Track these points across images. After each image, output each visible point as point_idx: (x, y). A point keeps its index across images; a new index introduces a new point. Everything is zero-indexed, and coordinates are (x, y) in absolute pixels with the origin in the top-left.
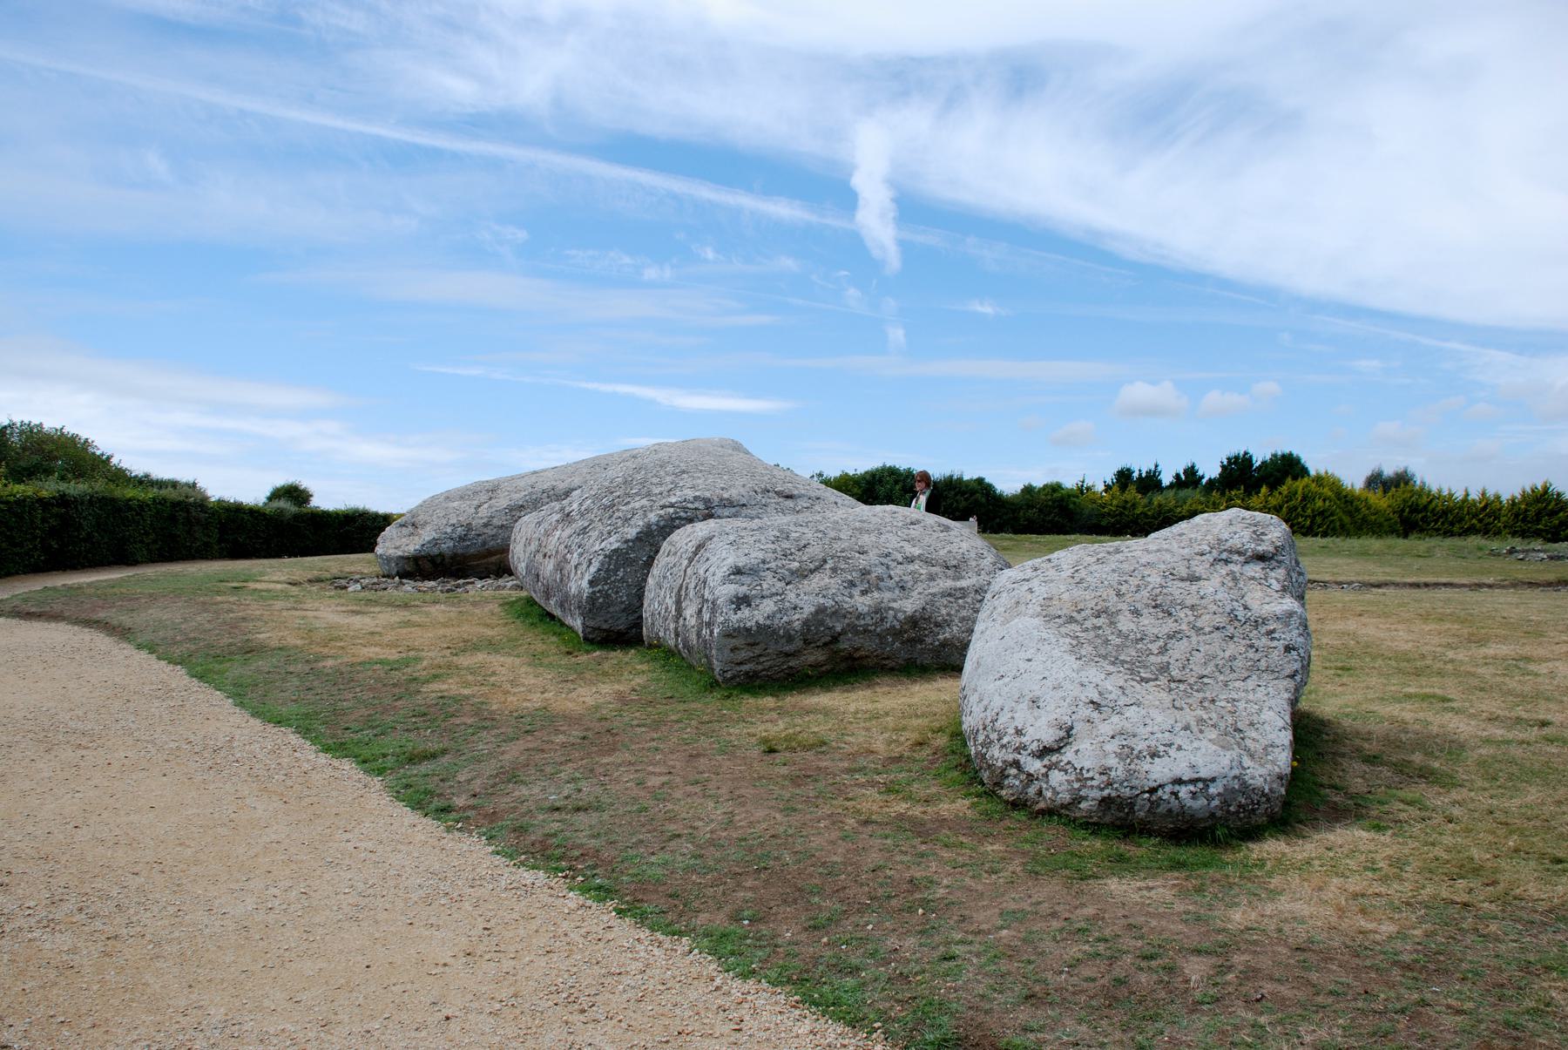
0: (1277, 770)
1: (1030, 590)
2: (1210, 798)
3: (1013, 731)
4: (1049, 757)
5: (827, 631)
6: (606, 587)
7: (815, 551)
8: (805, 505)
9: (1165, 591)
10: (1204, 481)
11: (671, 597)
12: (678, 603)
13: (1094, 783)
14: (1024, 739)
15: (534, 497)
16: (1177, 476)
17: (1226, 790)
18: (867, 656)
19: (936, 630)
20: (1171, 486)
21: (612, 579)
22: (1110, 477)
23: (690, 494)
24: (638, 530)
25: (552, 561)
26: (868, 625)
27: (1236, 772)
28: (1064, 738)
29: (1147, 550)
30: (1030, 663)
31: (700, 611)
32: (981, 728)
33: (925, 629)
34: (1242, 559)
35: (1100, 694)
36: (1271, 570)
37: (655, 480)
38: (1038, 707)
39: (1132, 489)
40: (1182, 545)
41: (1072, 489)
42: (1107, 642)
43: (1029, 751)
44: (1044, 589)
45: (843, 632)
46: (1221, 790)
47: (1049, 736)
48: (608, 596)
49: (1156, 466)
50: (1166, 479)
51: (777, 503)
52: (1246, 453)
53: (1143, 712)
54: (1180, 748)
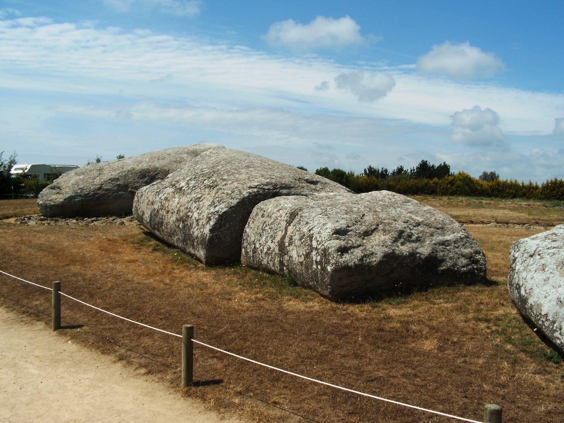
6: (219, 233)
7: (369, 218)
8: (321, 187)
15: (124, 174)
21: (223, 228)
24: (238, 201)
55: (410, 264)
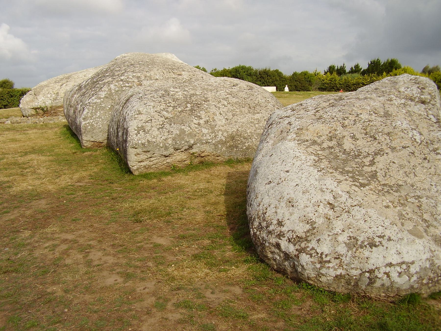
1: (290, 123)
5: (186, 143)
6: (91, 121)
9: (371, 124)
10: (362, 70)
13: (331, 265)
14: (283, 229)
16: (352, 68)
17: (421, 269)
18: (208, 155)
19: (244, 141)
20: (349, 73)
21: (94, 117)
22: (326, 69)
26: (208, 139)
29: (358, 98)
30: (288, 174)
33: (238, 140)
34: (413, 103)
35: (335, 198)
38: (293, 206)
39: (335, 74)
40: (379, 95)
41: (312, 74)
42: (336, 157)
44: (298, 123)
45: (195, 144)
46: (418, 269)
48: (92, 125)
49: (344, 65)
50: (348, 70)
52: (378, 60)
53: (363, 211)
54: (389, 239)
55: (211, 140)
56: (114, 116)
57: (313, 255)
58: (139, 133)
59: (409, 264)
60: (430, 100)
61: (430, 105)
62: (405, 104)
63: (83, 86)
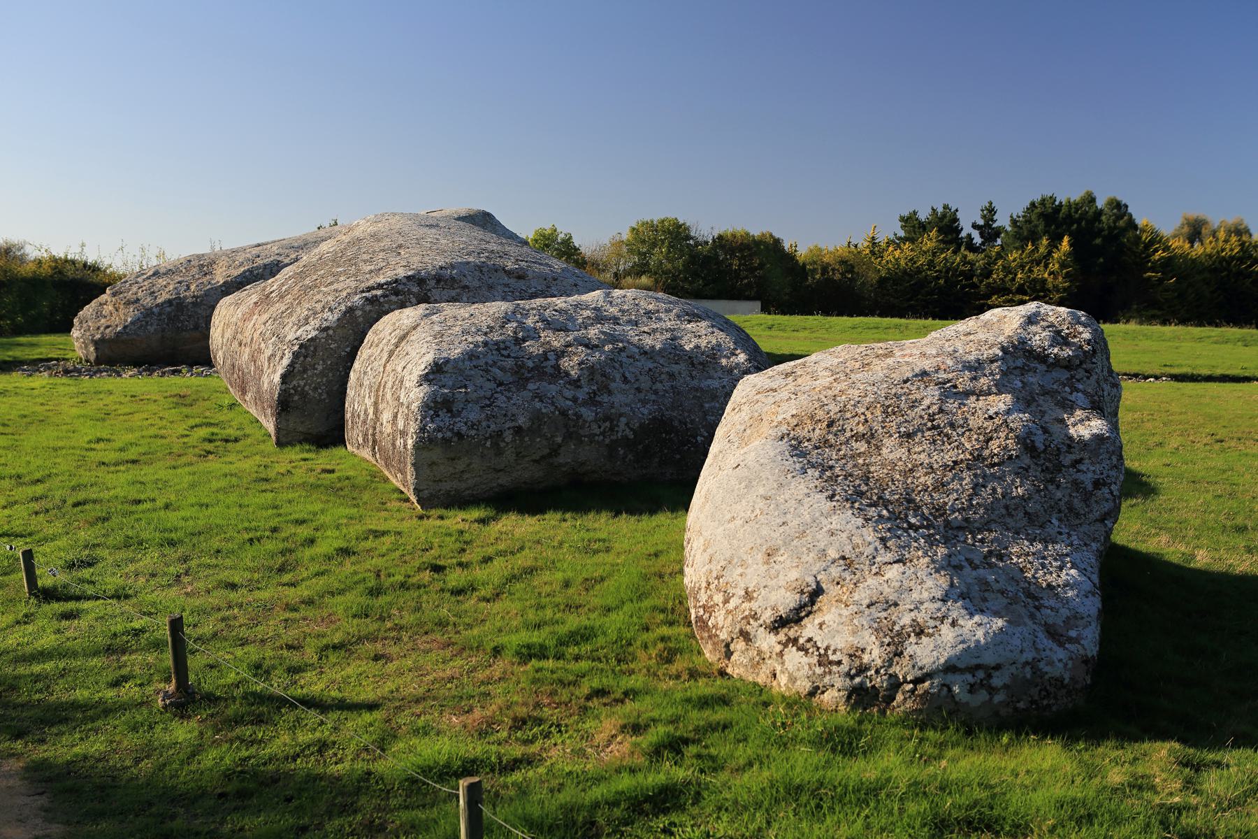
0: (1082, 652)
2: (992, 690)
3: (743, 593)
4: (786, 630)
6: (302, 383)
11: (369, 397)
12: (376, 404)
21: (310, 373)
23: (401, 273)
25: (248, 349)
27: (1028, 656)
28: (805, 605)
31: (395, 416)
32: (704, 585)
34: (1044, 367)
36: (1078, 381)
37: (365, 257)
43: (761, 622)
46: (1007, 680)
47: (786, 601)
51: (507, 285)
56: (365, 373)
57: (811, 651)
58: (438, 416)
59: (991, 670)
60: (1081, 363)
61: (1080, 370)
62: (1023, 368)
63: (273, 295)
